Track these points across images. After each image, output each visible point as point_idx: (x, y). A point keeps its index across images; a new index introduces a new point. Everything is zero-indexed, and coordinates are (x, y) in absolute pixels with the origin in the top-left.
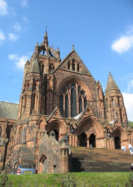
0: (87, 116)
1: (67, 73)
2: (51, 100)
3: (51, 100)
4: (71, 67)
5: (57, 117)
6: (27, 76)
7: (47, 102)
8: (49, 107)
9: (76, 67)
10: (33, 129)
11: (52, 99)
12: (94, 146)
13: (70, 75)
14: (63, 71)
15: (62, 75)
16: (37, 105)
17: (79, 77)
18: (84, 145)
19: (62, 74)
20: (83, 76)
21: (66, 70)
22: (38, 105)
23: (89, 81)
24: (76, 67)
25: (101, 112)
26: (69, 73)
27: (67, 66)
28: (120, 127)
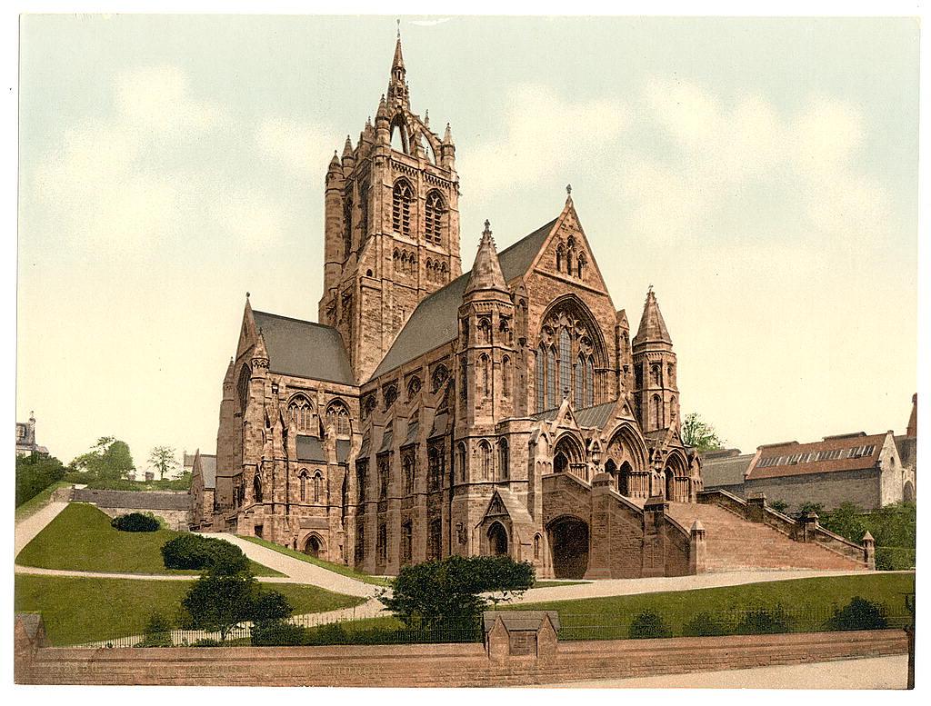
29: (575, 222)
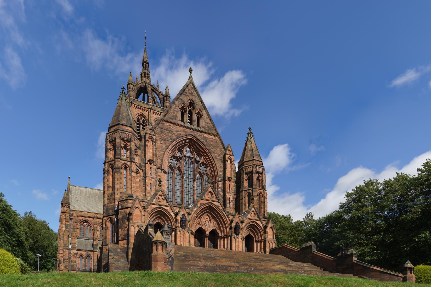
0: (207, 202)
1: (178, 128)
2: (154, 178)
3: (154, 178)
4: (187, 117)
5: (160, 203)
6: (110, 131)
7: (147, 181)
8: (151, 188)
9: (195, 117)
10: (125, 222)
11: (155, 177)
12: (215, 246)
13: (183, 133)
14: (172, 125)
15: (169, 133)
16: (245, 200)
17: (199, 138)
18: (202, 245)
19: (171, 131)
20: (205, 135)
21: (176, 122)
22: (244, 201)
23: (214, 145)
24: (195, 117)
25: (229, 198)
26: (182, 128)
27: (179, 115)
28: (256, 220)
29: (193, 90)
